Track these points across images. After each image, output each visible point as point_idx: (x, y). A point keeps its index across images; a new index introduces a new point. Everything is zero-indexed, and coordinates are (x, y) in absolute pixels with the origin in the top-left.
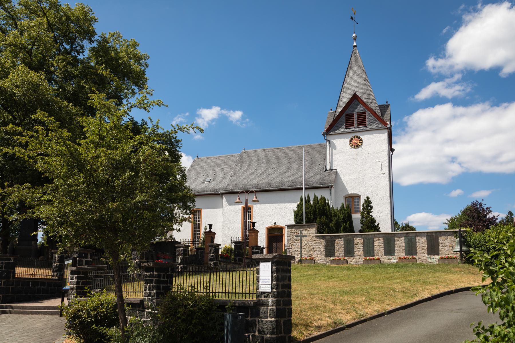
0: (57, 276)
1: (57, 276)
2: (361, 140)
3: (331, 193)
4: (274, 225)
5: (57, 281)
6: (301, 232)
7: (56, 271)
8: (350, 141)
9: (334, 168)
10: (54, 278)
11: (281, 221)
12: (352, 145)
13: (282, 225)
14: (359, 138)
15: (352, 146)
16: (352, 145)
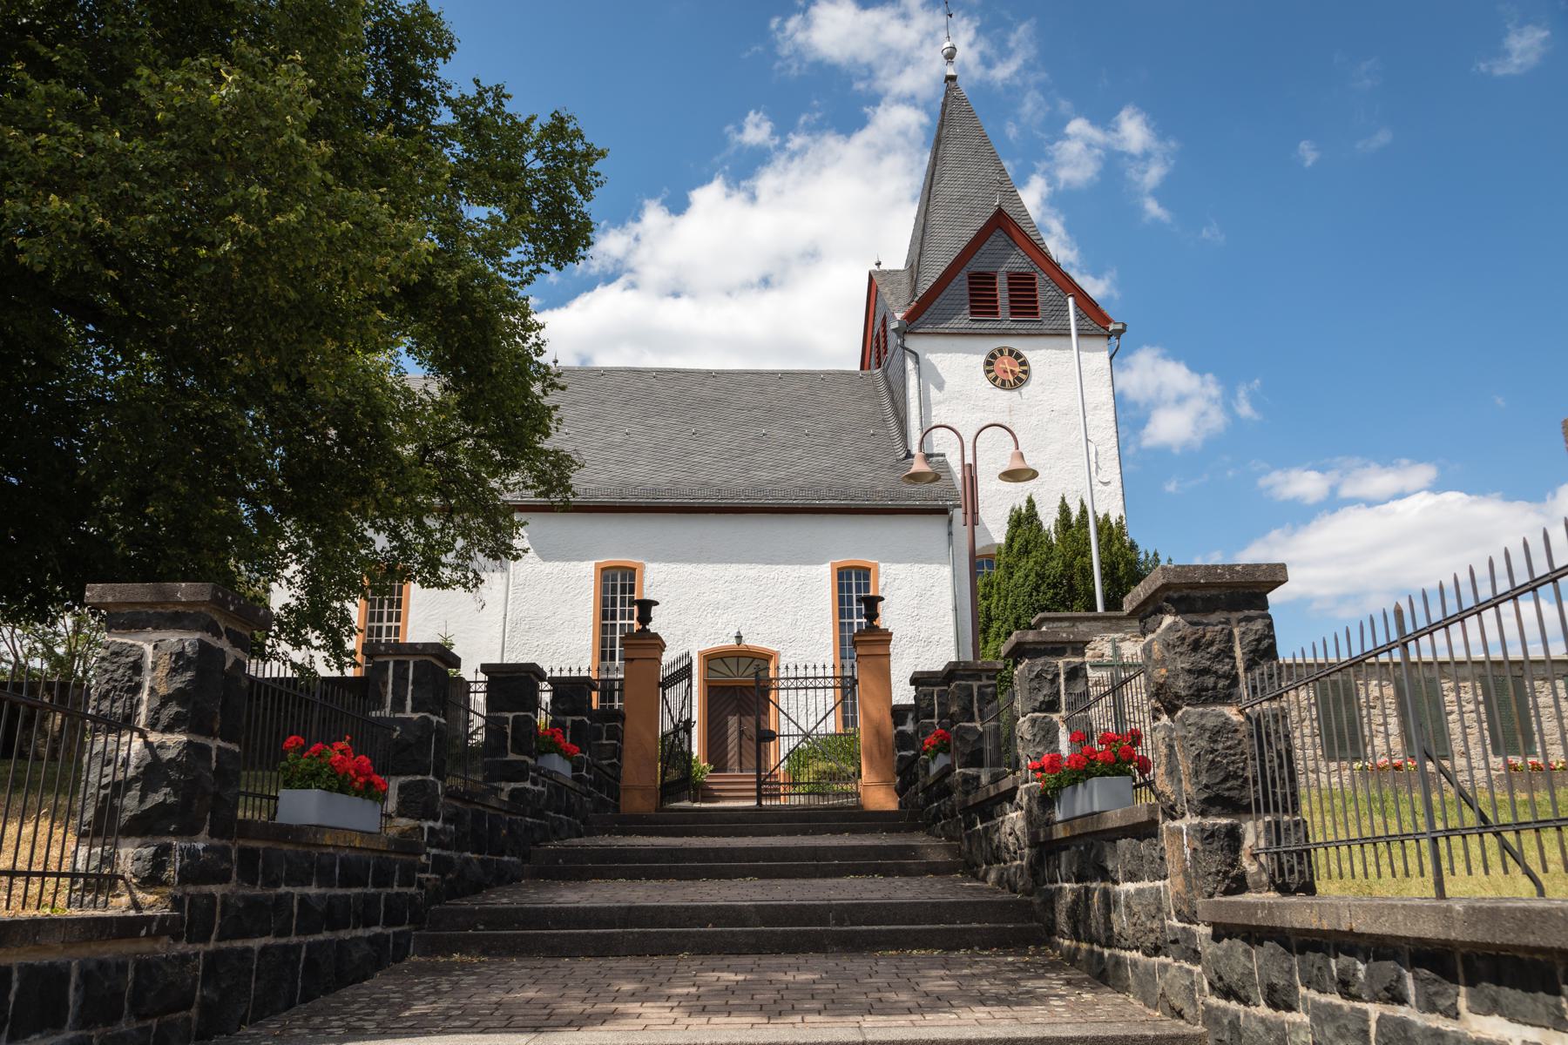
0: (151, 881)
1: (151, 881)
2: (1024, 363)
3: (950, 534)
4: (733, 642)
5: (164, 948)
6: (1116, 649)
7: (141, 826)
8: (988, 363)
9: (935, 451)
10: (119, 905)
11: (760, 629)
12: (996, 378)
13: (764, 646)
14: (1018, 356)
15: (995, 379)
16: (996, 378)
